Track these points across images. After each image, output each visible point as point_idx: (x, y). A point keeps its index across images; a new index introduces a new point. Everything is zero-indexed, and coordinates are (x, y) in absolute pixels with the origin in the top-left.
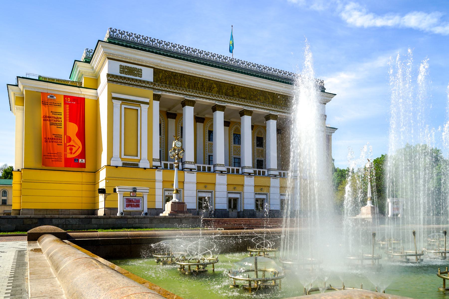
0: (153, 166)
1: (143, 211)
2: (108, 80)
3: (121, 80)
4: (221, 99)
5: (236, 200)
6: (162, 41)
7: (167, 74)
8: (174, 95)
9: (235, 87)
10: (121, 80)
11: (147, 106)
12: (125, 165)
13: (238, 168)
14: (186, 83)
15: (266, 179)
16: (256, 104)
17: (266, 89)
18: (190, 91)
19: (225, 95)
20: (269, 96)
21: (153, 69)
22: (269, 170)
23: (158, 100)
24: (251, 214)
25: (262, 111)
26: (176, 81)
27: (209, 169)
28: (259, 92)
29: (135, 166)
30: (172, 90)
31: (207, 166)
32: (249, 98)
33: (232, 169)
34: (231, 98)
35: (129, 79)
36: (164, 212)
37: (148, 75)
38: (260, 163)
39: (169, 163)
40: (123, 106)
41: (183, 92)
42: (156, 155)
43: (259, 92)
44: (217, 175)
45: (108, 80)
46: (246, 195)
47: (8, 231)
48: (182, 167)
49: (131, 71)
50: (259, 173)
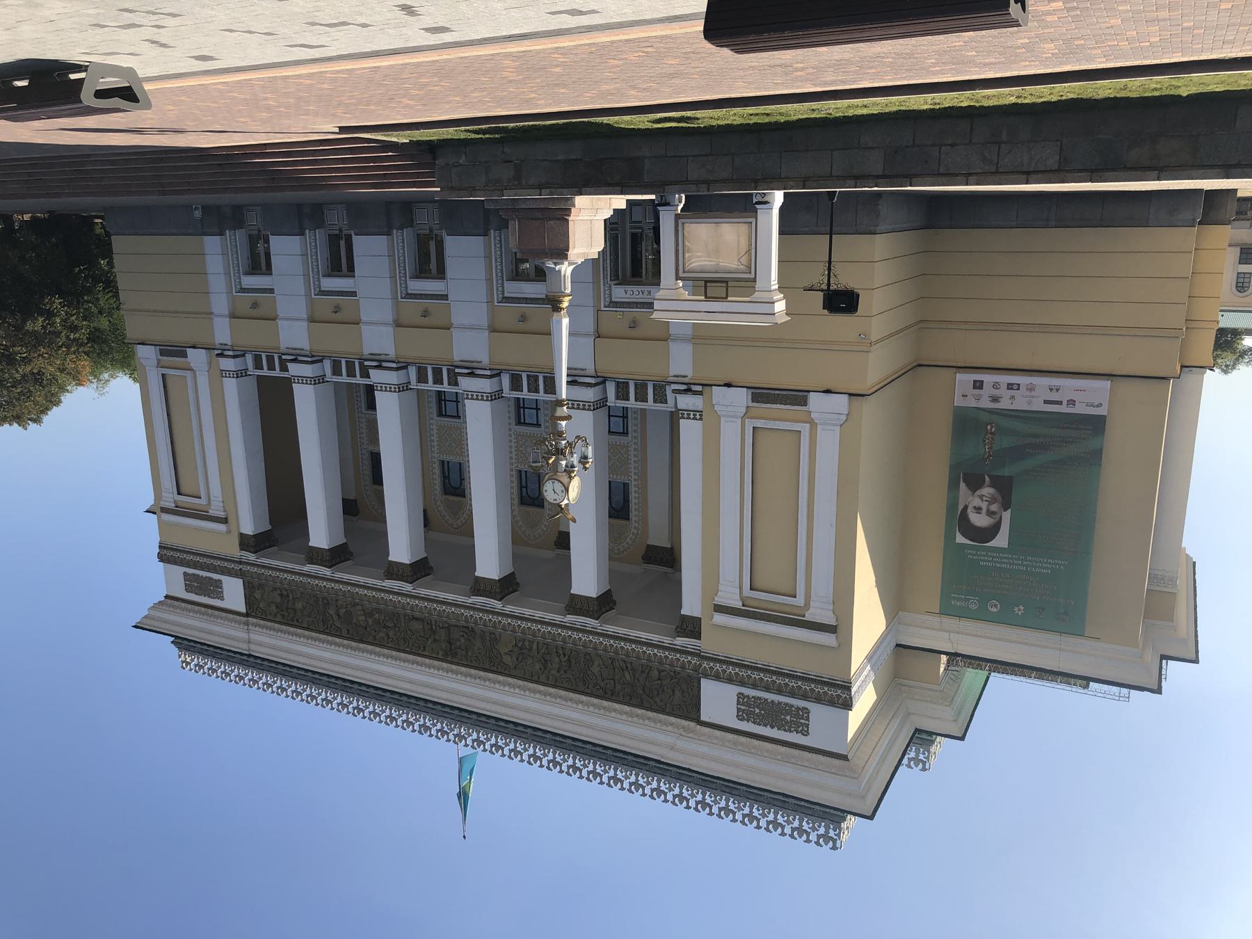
0: (700, 393)
1: (677, 217)
2: (847, 688)
3: (806, 687)
6: (673, 803)
7: (657, 700)
8: (634, 634)
9: (446, 654)
10: (806, 687)
11: (721, 600)
12: (798, 397)
14: (595, 669)
15: (607, 368)
16: (377, 601)
17: (371, 653)
18: (627, 655)
19: (473, 630)
20: (338, 624)
21: (703, 718)
22: (496, 396)
23: (685, 618)
24: (461, 218)
25: (355, 579)
26: (628, 677)
27: (622, 392)
28: (370, 639)
29: (761, 395)
30: (639, 649)
31: (632, 403)
33: (537, 391)
34: (453, 622)
35: (780, 691)
36: (608, 214)
37: (718, 700)
39: (430, 386)
40: (800, 600)
41: (606, 642)
42: (690, 431)
43: (370, 639)
44: (485, 361)
45: (849, 689)
46: (383, 287)
47: (729, 130)
48: (605, 390)
49: (773, 715)
50: (533, 381)
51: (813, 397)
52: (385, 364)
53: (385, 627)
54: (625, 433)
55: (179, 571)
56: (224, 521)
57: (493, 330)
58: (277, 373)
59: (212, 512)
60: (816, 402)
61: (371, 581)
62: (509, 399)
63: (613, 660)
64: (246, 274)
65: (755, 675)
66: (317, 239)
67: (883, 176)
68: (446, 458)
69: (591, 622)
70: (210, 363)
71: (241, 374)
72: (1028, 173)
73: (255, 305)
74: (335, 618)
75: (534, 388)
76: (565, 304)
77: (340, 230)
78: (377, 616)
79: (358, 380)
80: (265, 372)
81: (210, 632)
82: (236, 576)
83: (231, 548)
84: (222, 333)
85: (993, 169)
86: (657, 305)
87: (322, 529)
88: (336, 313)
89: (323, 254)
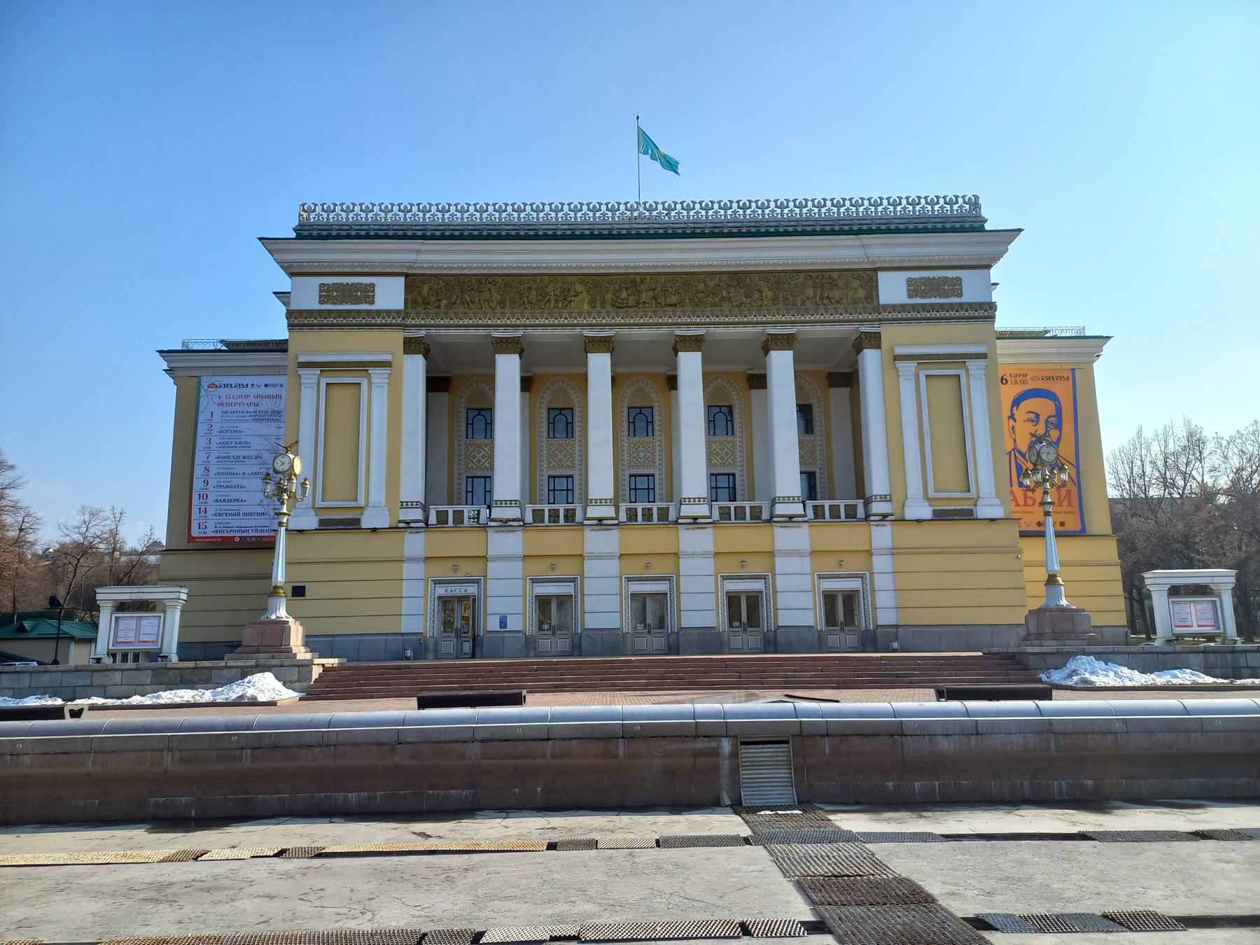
0: (400, 522)
4: (599, 321)
5: (754, 600)
12: (941, 516)
13: (664, 505)
14: (497, 296)
21: (402, 279)
31: (546, 507)
32: (692, 300)
33: (567, 510)
37: (390, 295)
38: (724, 485)
52: (412, 525)
56: (897, 358)
57: (485, 558)
59: (913, 365)
60: (927, 513)
65: (359, 320)
83: (889, 333)
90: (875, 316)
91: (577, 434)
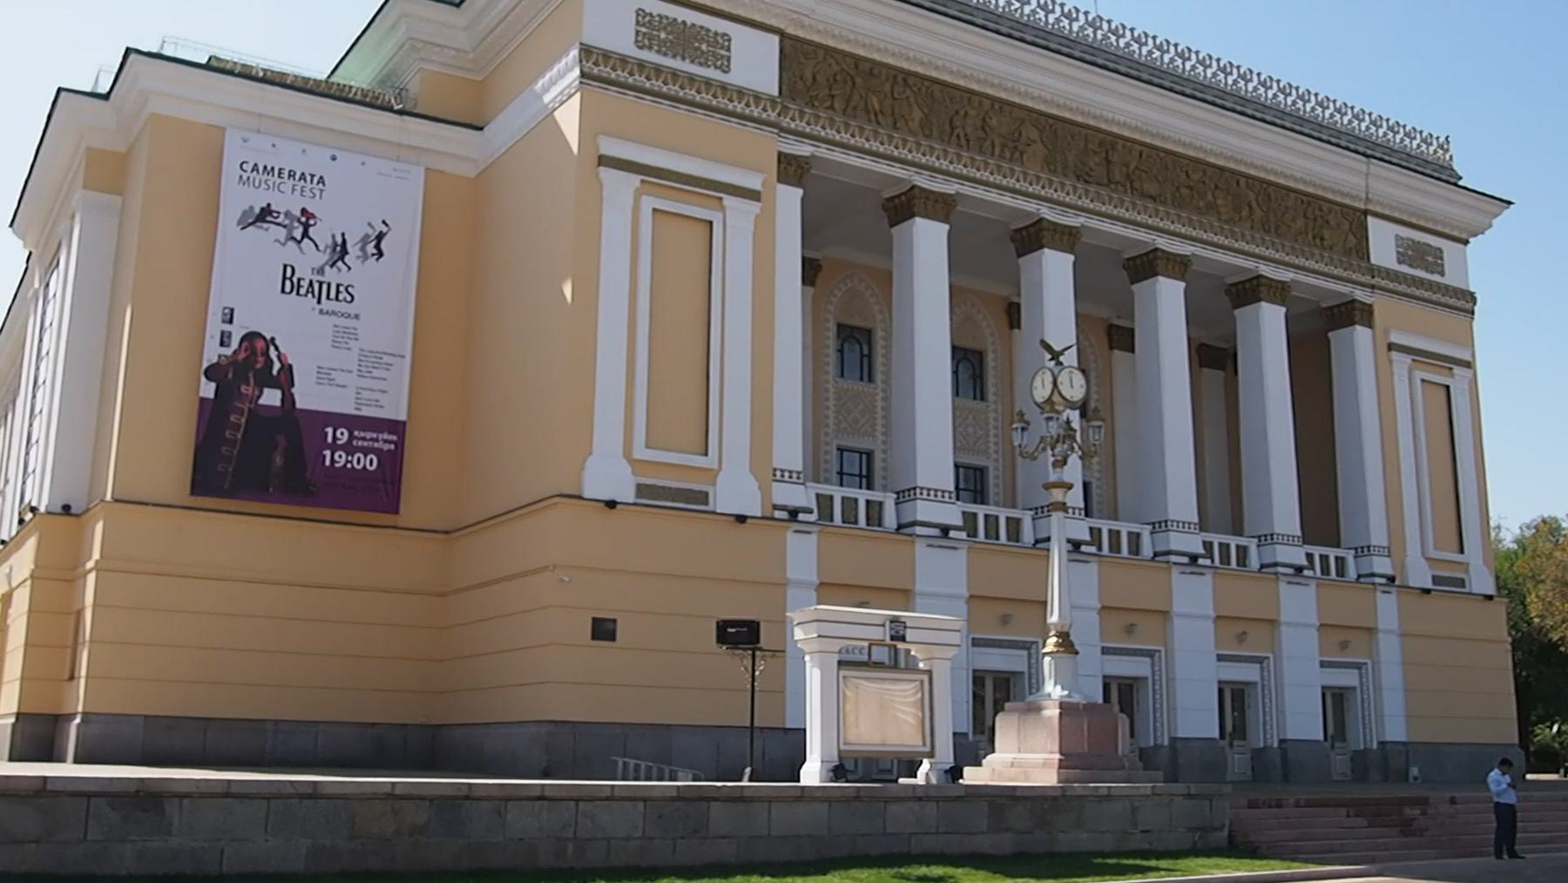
0: (775, 507)
8: (866, 163)
9: (1113, 146)
11: (754, 207)
14: (917, 115)
19: (1078, 178)
23: (798, 183)
39: (1124, 528)
42: (790, 450)
43: (1210, 171)
44: (920, 548)
45: (583, 75)
49: (684, 40)
51: (628, 495)
53: (1191, 188)
54: (841, 450)
55: (1449, 279)
56: (1391, 347)
58: (1317, 551)
59: (1408, 359)
61: (838, 156)
62: (885, 489)
63: (895, 127)
64: (1253, 684)
65: (706, 98)
66: (1262, 735)
67: (709, 799)
68: (862, 387)
69: (923, 181)
70: (1403, 567)
71: (1363, 551)
72: (541, 798)
73: (1241, 638)
74: (1254, 204)
75: (850, 504)
76: (1052, 640)
77: (1231, 745)
78: (1202, 204)
79: (1105, 526)
80: (1332, 553)
81: (1241, 134)
82: (1379, 268)
84: (1387, 608)
85: (581, 805)
86: (909, 635)
87: (1268, 329)
88: (1245, 630)
89: (1255, 717)
90: (1367, 279)
91: (879, 377)
